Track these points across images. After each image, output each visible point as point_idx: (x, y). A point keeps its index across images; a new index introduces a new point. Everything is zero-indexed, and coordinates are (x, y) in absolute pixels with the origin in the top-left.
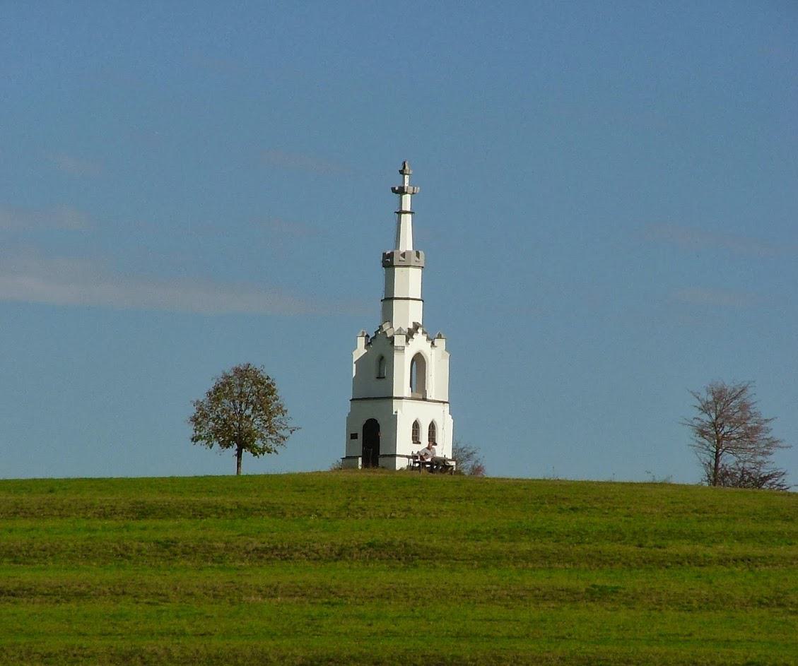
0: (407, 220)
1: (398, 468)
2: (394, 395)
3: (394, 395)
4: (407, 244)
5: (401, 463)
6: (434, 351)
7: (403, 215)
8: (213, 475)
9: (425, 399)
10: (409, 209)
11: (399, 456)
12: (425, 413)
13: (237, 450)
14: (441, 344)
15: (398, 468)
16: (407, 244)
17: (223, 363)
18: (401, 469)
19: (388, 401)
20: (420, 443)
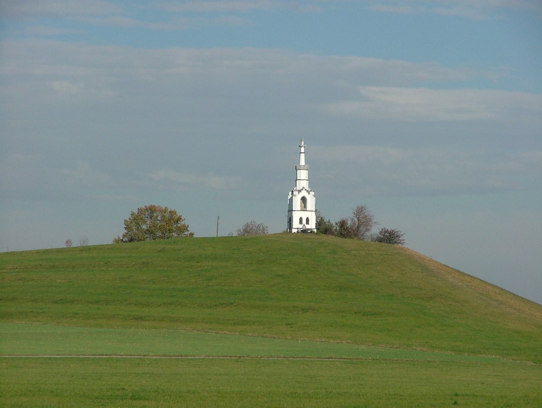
0: (303, 156)
1: (293, 232)
2: (293, 210)
3: (293, 210)
4: (302, 162)
5: (294, 231)
6: (309, 195)
7: (301, 154)
8: (222, 236)
9: (306, 211)
10: (303, 152)
11: (217, 236)
12: (304, 215)
13: (333, 224)
14: (312, 193)
15: (293, 232)
16: (302, 162)
17: (307, 217)
18: (294, 233)
19: (291, 211)
20: (309, 224)
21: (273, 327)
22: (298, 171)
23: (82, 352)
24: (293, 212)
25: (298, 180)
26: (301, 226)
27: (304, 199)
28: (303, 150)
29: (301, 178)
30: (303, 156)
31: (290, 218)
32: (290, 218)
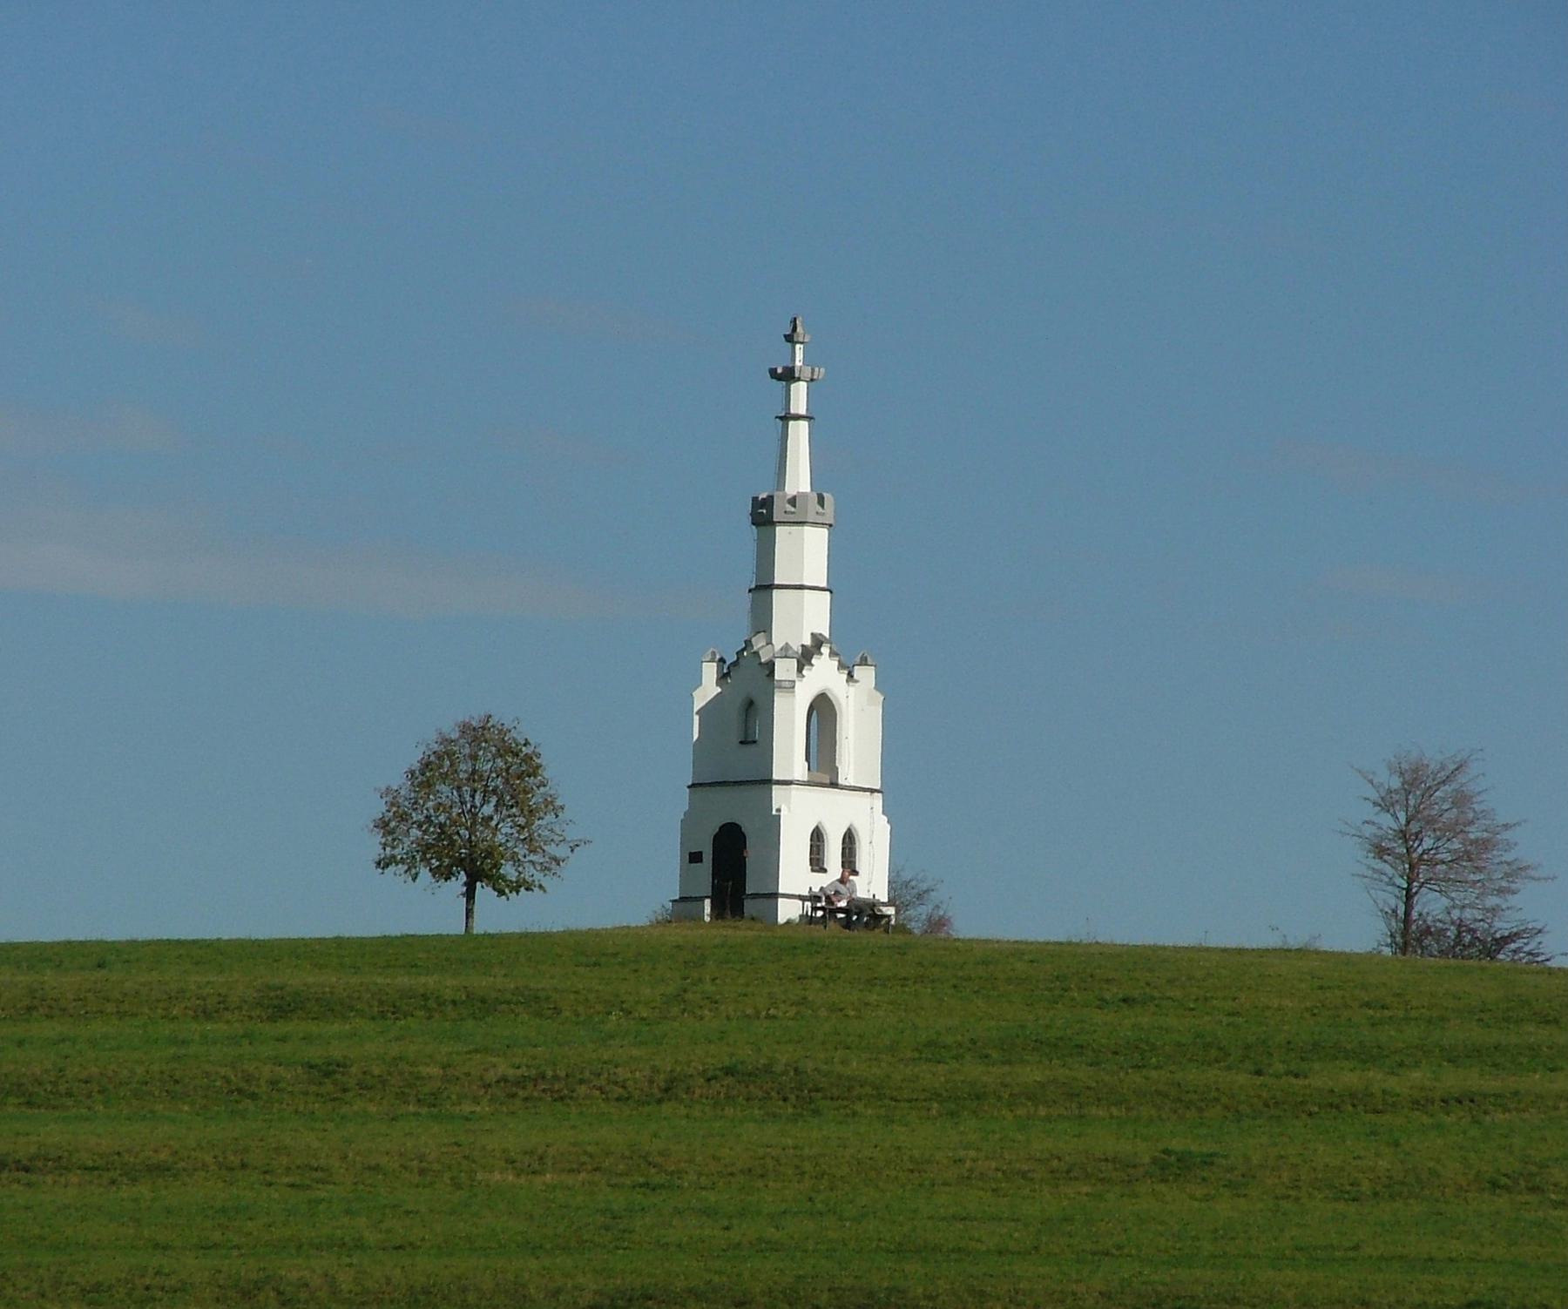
0: (799, 433)
1: (781, 919)
2: (775, 777)
3: (775, 777)
4: (799, 479)
7: (791, 423)
9: (834, 785)
10: (803, 411)
14: (866, 675)
15: (781, 919)
16: (799, 479)
18: (789, 922)
21: (138, 1086)
22: (801, 902)
23: (776, 1251)
24: (776, 790)
25: (803, 904)
26: (819, 882)
27: (822, 711)
28: (799, 403)
29: (801, 578)
30: (799, 433)
31: (750, 704)
32: (750, 704)
